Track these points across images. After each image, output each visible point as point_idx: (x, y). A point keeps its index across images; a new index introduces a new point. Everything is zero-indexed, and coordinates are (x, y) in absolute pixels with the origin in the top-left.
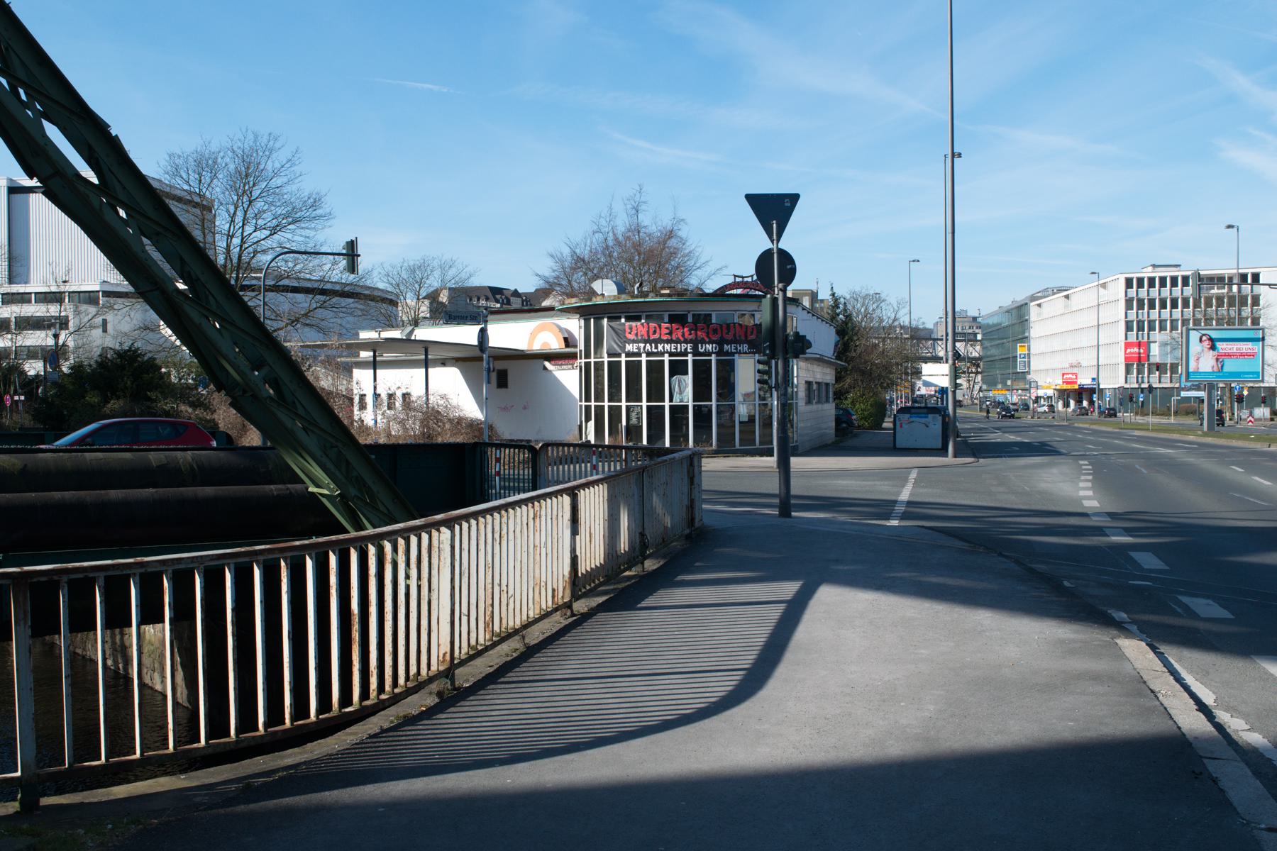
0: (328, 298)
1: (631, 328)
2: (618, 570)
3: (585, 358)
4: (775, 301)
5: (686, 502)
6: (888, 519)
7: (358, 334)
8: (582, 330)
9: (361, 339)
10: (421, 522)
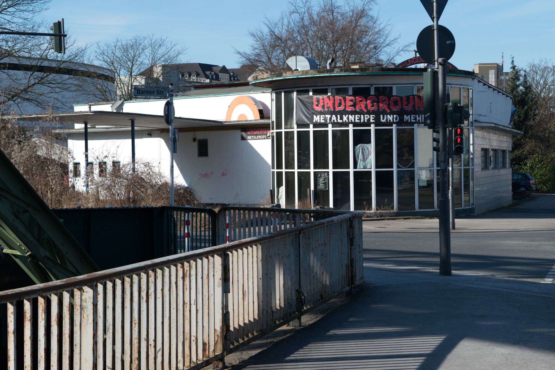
0: (45, 75)
1: (318, 101)
2: (273, 325)
3: (277, 129)
4: (435, 74)
5: (346, 261)
6: (543, 276)
7: (72, 108)
8: (274, 103)
9: (77, 112)
10: (62, 282)
